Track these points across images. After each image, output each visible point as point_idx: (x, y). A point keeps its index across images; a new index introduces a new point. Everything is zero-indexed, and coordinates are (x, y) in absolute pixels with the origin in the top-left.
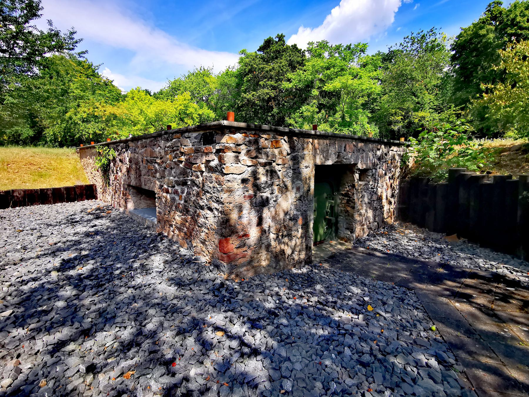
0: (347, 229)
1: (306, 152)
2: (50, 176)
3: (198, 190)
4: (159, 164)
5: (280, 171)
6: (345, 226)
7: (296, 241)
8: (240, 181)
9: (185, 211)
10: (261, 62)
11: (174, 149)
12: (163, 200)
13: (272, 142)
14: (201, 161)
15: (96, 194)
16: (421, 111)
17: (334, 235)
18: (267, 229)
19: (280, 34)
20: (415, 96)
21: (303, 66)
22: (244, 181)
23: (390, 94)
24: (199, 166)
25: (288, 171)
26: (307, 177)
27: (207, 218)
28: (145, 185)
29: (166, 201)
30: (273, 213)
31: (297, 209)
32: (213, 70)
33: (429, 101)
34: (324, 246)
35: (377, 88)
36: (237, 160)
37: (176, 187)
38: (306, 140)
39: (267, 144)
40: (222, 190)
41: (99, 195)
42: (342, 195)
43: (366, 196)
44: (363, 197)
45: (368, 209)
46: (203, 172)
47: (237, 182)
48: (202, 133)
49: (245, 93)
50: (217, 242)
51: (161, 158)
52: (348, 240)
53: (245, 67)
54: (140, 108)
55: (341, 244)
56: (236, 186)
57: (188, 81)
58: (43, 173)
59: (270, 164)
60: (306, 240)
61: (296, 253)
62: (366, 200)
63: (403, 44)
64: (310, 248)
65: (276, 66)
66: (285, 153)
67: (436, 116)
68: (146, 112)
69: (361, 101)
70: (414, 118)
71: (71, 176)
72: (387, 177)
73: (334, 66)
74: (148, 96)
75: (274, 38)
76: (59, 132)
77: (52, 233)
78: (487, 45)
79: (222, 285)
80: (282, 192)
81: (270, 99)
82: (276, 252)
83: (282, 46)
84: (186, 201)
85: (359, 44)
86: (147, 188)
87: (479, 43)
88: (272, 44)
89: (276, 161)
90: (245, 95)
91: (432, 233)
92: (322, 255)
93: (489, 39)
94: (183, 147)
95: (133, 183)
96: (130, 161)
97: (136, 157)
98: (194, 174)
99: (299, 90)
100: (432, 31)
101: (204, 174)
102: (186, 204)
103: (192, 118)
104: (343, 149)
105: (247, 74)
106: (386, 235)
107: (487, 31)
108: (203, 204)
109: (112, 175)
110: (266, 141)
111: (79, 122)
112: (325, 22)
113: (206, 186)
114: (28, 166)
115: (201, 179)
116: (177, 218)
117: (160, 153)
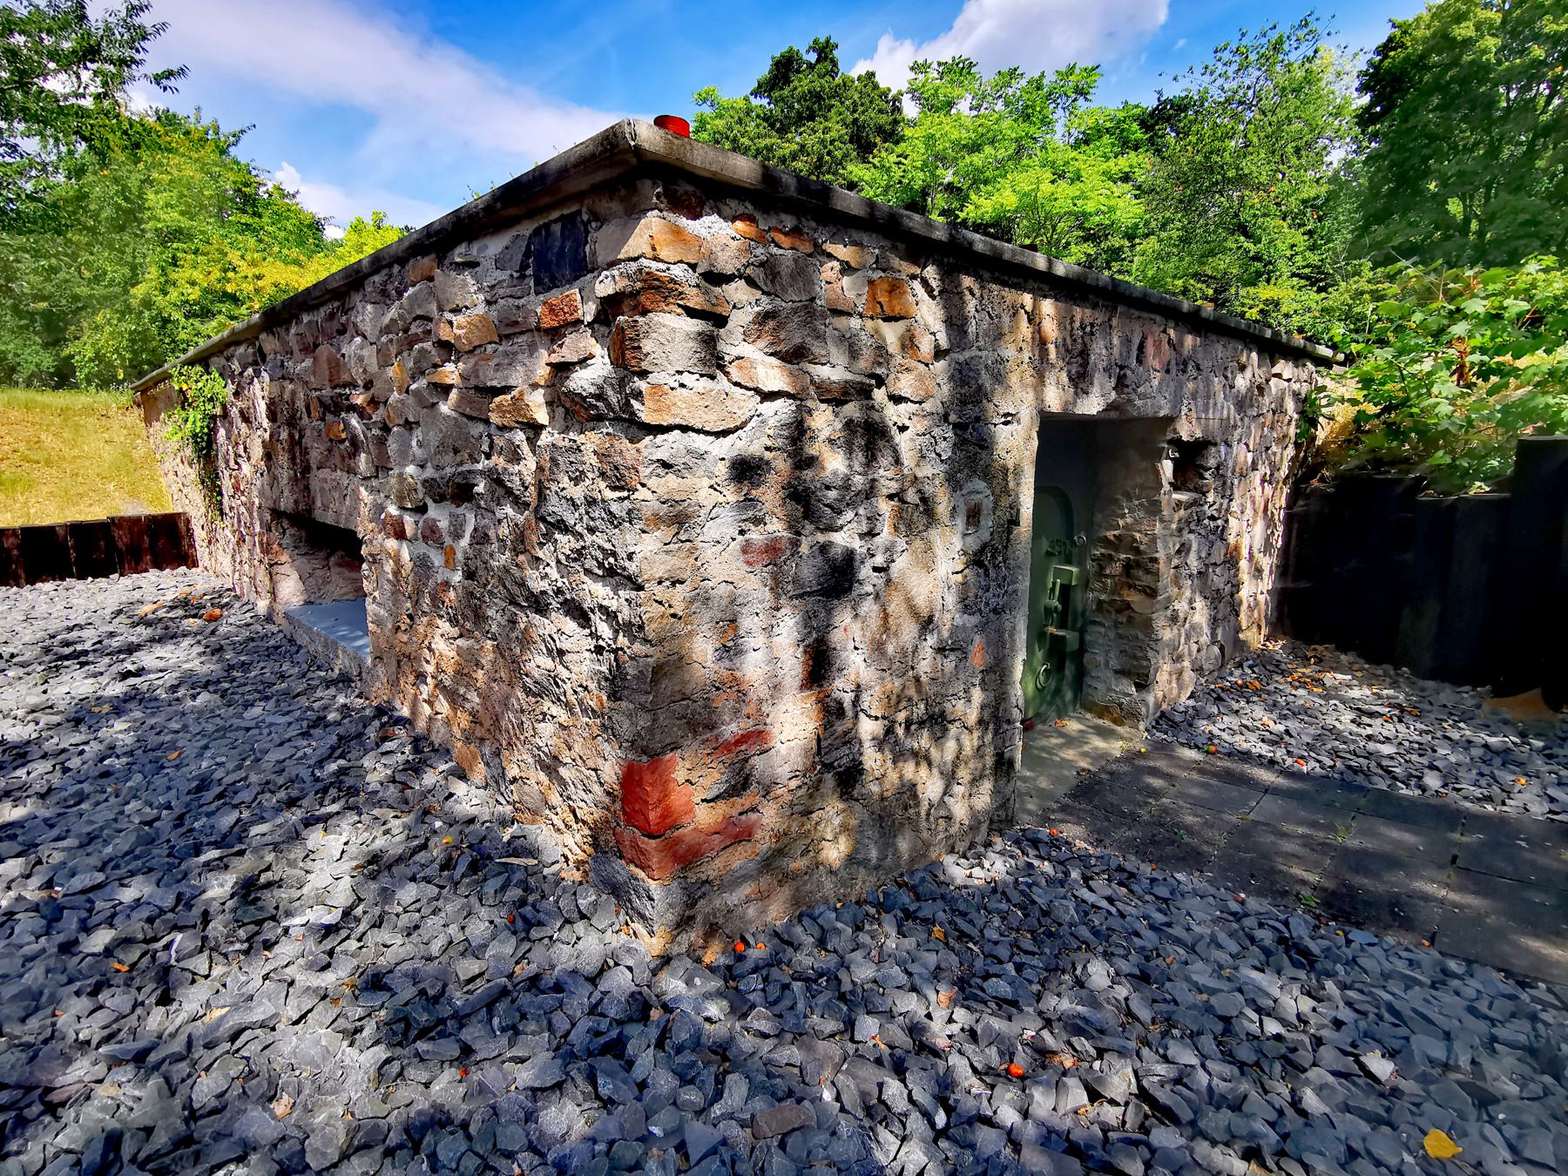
0: (1122, 673)
2: (30, 485)
3: (520, 519)
4: (361, 412)
5: (903, 429)
6: (1115, 663)
7: (962, 742)
8: (722, 470)
9: (471, 616)
12: (389, 567)
13: (871, 283)
14: (530, 372)
15: (192, 546)
16: (1268, 281)
17: (1069, 696)
18: (847, 699)
19: (822, 40)
20: (1247, 236)
21: (897, 143)
22: (745, 470)
23: (1164, 235)
25: (937, 431)
26: (1011, 465)
27: (561, 653)
29: (396, 573)
30: (875, 623)
31: (966, 606)
33: (1288, 253)
34: (1044, 742)
35: (1128, 209)
36: (713, 361)
37: (433, 512)
38: (1010, 295)
39: (850, 295)
40: (631, 515)
41: (201, 551)
43: (1194, 547)
44: (1183, 550)
45: (1198, 598)
50: (610, 772)
51: (368, 385)
52: (1129, 715)
55: (1104, 733)
56: (706, 497)
59: (864, 393)
60: (996, 733)
61: (958, 790)
62: (1194, 563)
64: (1011, 763)
66: (926, 346)
67: (1312, 297)
70: (1243, 305)
71: (111, 486)
72: (1256, 477)
73: (992, 142)
75: (803, 52)
76: (116, 351)
78: (1481, 71)
79: (640, 1006)
80: (909, 527)
82: (883, 799)
83: (828, 78)
84: (470, 575)
85: (1071, 70)
86: (329, 519)
87: (1448, 67)
88: (798, 71)
89: (890, 381)
91: (1431, 684)
92: (1043, 783)
93: (1485, 52)
94: (448, 316)
95: (286, 503)
96: (272, 416)
97: (286, 396)
98: (499, 442)
100: (1306, 25)
101: (545, 439)
106: (1257, 692)
107: (1478, 27)
108: (543, 585)
109: (227, 474)
110: (846, 281)
111: (176, 315)
112: (959, 23)
113: (553, 499)
115: (529, 464)
116: (440, 645)
117: (361, 359)
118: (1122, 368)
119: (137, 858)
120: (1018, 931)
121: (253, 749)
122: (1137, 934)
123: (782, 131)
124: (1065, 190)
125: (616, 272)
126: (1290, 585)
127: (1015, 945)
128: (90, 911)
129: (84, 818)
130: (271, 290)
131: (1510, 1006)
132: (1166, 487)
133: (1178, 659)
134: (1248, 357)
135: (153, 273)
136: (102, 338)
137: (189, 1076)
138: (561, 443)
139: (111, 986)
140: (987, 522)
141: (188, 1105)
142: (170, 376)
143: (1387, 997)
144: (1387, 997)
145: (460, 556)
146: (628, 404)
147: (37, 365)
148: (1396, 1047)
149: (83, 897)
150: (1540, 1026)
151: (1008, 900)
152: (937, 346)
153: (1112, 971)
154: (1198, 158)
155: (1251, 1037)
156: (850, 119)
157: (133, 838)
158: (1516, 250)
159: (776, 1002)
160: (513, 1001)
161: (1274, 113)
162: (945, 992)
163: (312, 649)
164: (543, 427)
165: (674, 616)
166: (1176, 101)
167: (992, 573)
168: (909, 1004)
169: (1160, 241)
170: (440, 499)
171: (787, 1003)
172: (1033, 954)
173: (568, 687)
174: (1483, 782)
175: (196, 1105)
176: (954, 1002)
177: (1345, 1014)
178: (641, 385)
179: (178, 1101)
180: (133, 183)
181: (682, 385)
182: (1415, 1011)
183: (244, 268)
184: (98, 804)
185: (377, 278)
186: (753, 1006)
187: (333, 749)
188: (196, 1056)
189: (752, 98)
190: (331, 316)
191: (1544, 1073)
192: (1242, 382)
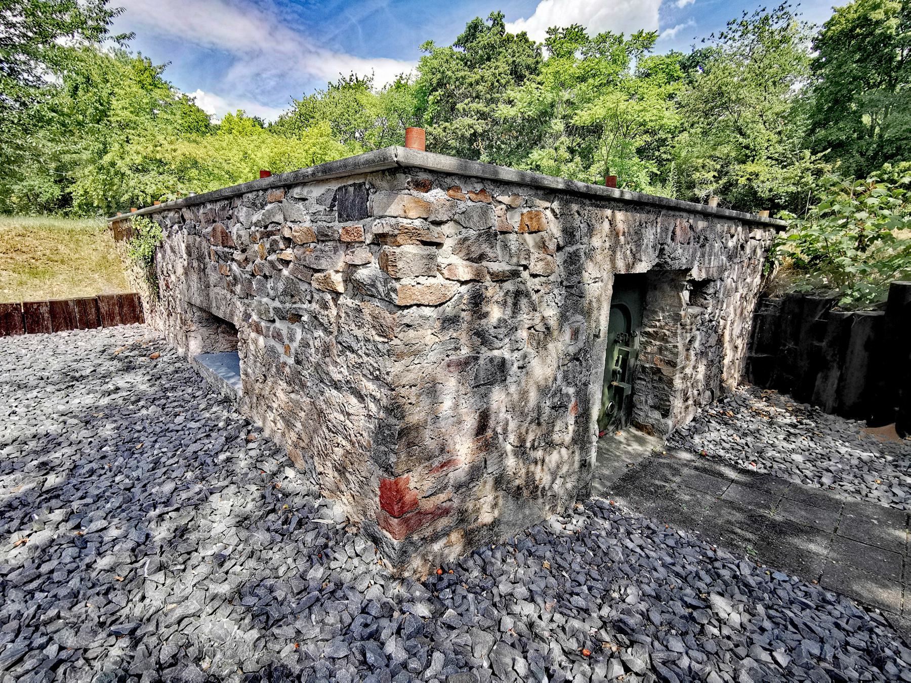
0: (655, 407)
1: (596, 242)
2: (53, 275)
3: (327, 339)
6: (650, 402)
9: (296, 382)
10: (461, 67)
11: (269, 228)
15: (141, 312)
16: (753, 161)
19: (496, 13)
20: (741, 134)
21: (538, 75)
23: (692, 131)
24: (327, 278)
27: (349, 414)
32: (373, 82)
33: (766, 145)
37: (278, 324)
41: (147, 315)
42: (648, 334)
43: (699, 338)
46: (338, 294)
47: (432, 328)
48: (334, 186)
49: (431, 126)
51: (243, 251)
53: (431, 76)
54: (242, 148)
55: (641, 441)
57: (328, 101)
58: (40, 268)
63: (725, 34)
65: (488, 74)
67: (778, 171)
68: (253, 156)
69: (639, 142)
70: (737, 175)
74: (258, 127)
75: (484, 20)
77: (14, 413)
84: (298, 362)
88: (481, 31)
90: (430, 129)
91: (831, 417)
93: (889, 28)
95: (197, 300)
96: (189, 254)
98: (316, 297)
99: (528, 121)
101: (341, 300)
102: (299, 368)
104: (670, 234)
105: (435, 90)
107: (886, 13)
111: (128, 172)
113: (346, 334)
114: (10, 255)
115: (334, 311)
118: (662, 244)
119: (123, 511)
120: (590, 564)
121: (181, 444)
122: (656, 570)
123: (472, 67)
124: (634, 105)
125: (383, 222)
126: (753, 355)
127: (588, 574)
128: (101, 543)
129: (95, 485)
130: (181, 158)
131: (859, 622)
132: (685, 306)
133: (686, 400)
134: (736, 230)
135: (116, 146)
136: (88, 183)
137: (158, 644)
138: (350, 305)
139: (115, 589)
140: (582, 338)
141: (158, 663)
142: (130, 220)
143: (791, 615)
144: (791, 615)
145: (293, 351)
146: (388, 293)
147: (52, 194)
148: (793, 646)
149: (97, 535)
150: (874, 636)
151: (586, 545)
152: (558, 245)
153: (640, 592)
154: (714, 88)
155: (714, 637)
156: (510, 60)
157: (121, 499)
158: (900, 146)
159: (459, 606)
160: (322, 605)
161: (761, 61)
162: (551, 603)
163: (209, 380)
164: (341, 294)
165: (410, 404)
166: (704, 52)
167: (584, 364)
168: (528, 609)
169: (691, 135)
170: (283, 318)
171: (465, 607)
172: (598, 580)
173: (351, 432)
174: (856, 481)
175: (162, 662)
176: (554, 610)
177: (767, 624)
178: (397, 285)
179: (153, 660)
180: (104, 94)
181: (418, 283)
182: (805, 624)
183: (167, 146)
184: (101, 475)
185: (250, 195)
186: (447, 608)
187: (224, 445)
188: (161, 632)
189: (454, 48)
190: (223, 208)
191: (873, 665)
192: (731, 244)
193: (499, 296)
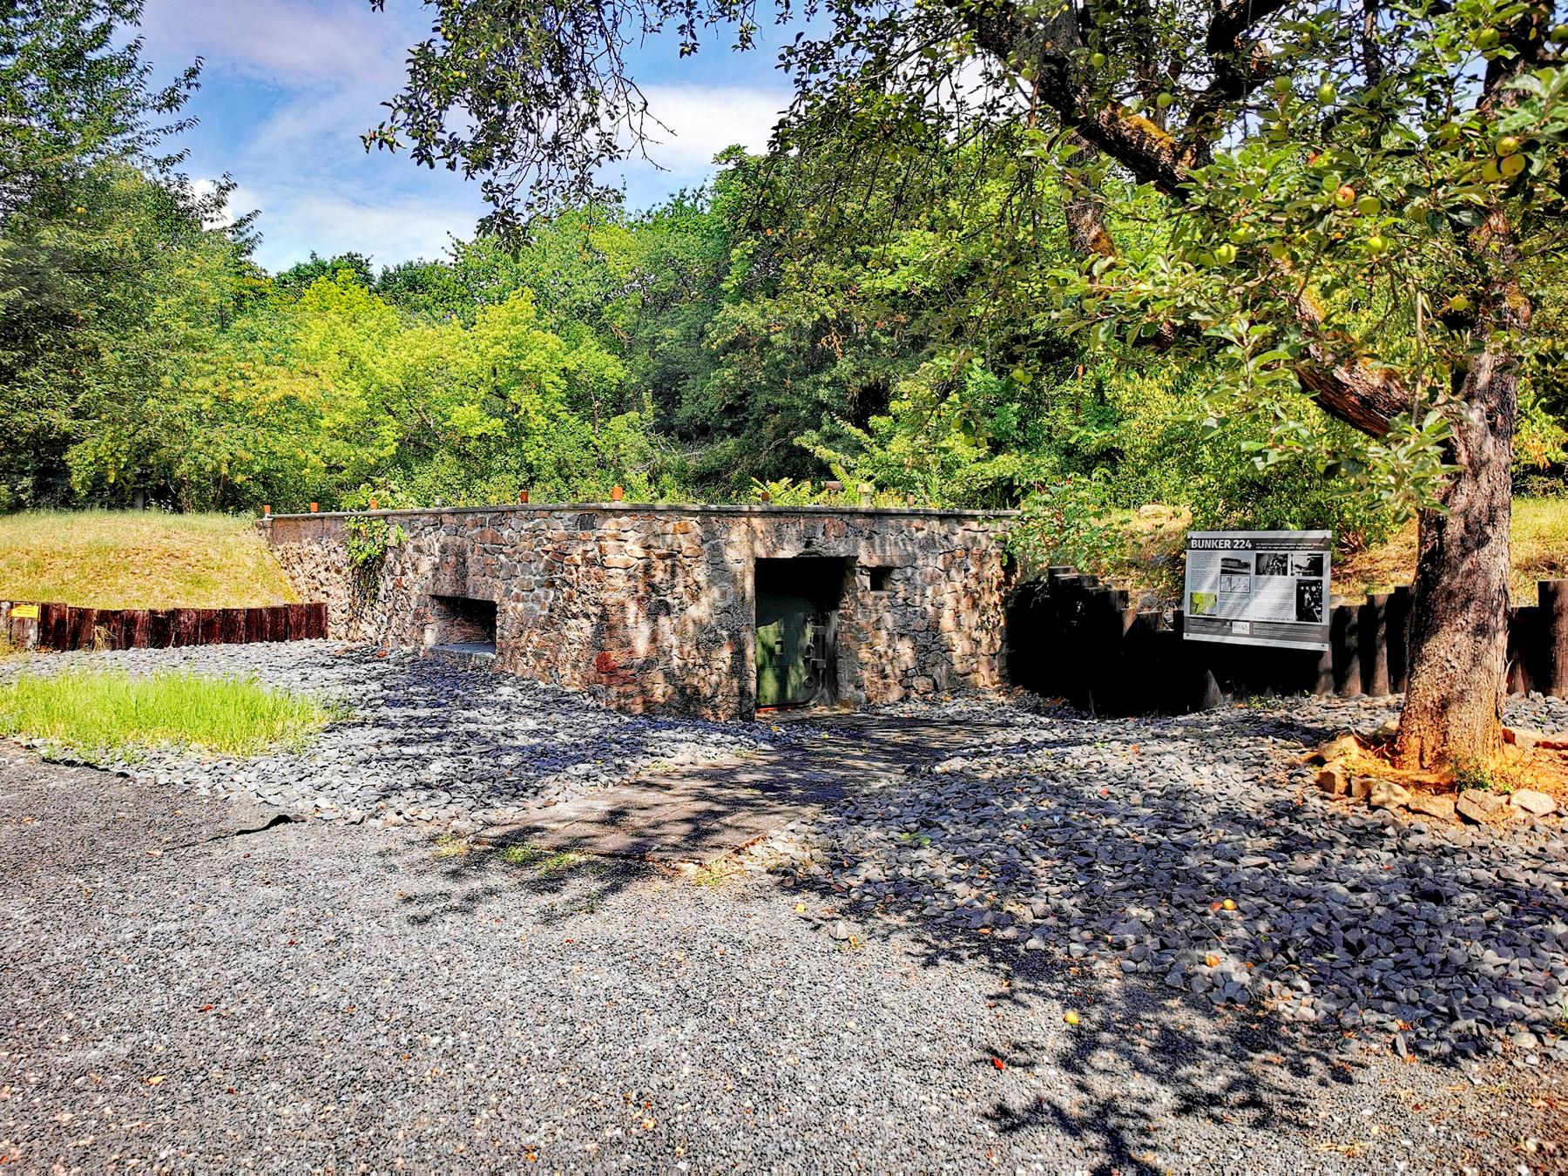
4: (507, 555)
28: (476, 592)
68: (370, 365)
81: (822, 327)
103: (540, 390)
193: (662, 566)
